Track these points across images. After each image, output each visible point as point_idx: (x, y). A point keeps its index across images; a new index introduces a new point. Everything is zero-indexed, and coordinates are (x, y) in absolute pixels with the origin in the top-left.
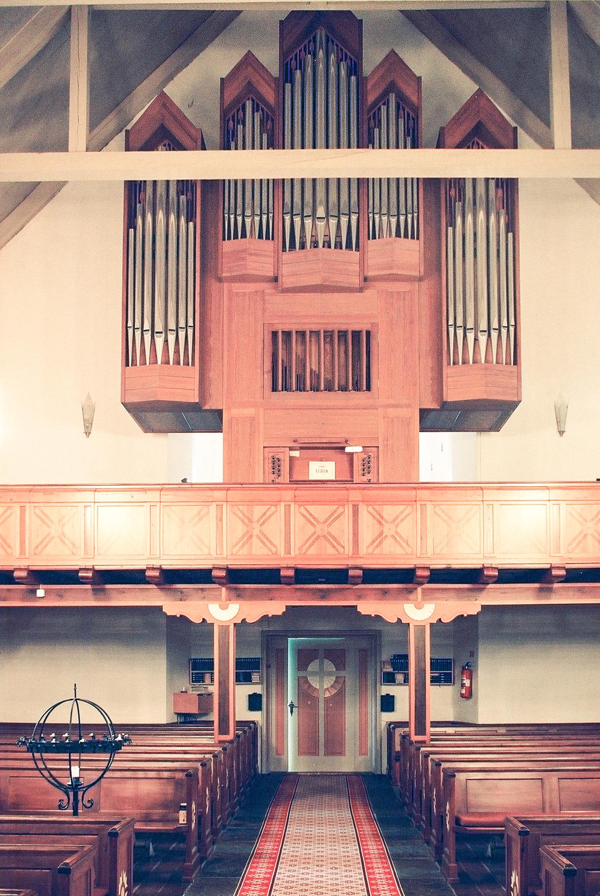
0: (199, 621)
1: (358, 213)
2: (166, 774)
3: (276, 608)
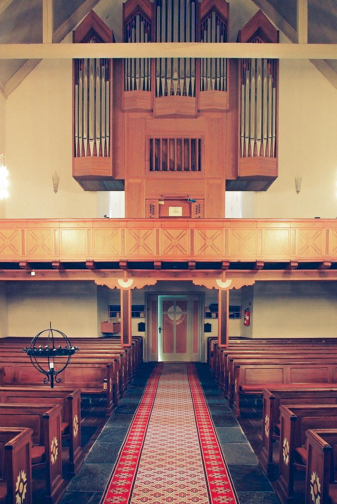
0: (113, 288)
1: (195, 76)
2: (97, 365)
3: (152, 281)
